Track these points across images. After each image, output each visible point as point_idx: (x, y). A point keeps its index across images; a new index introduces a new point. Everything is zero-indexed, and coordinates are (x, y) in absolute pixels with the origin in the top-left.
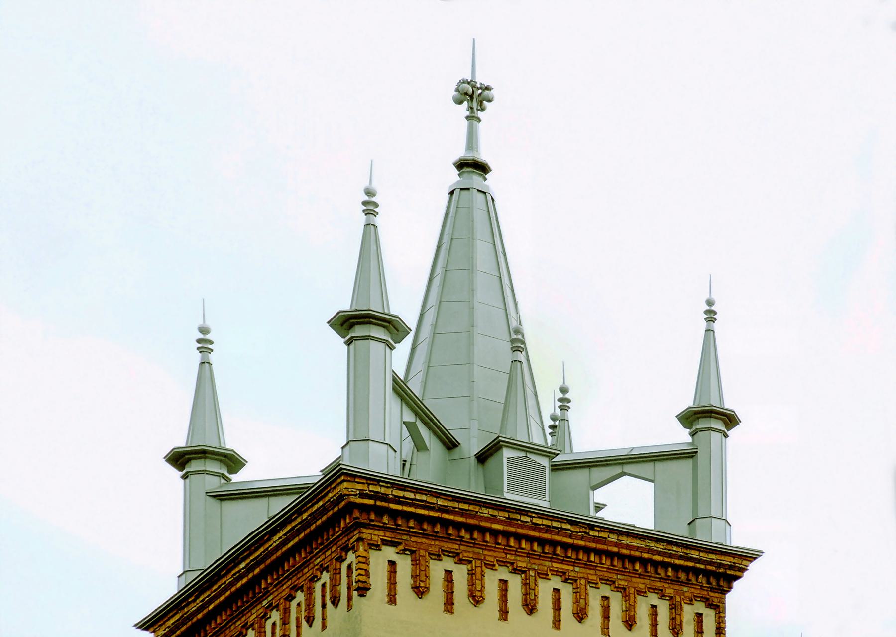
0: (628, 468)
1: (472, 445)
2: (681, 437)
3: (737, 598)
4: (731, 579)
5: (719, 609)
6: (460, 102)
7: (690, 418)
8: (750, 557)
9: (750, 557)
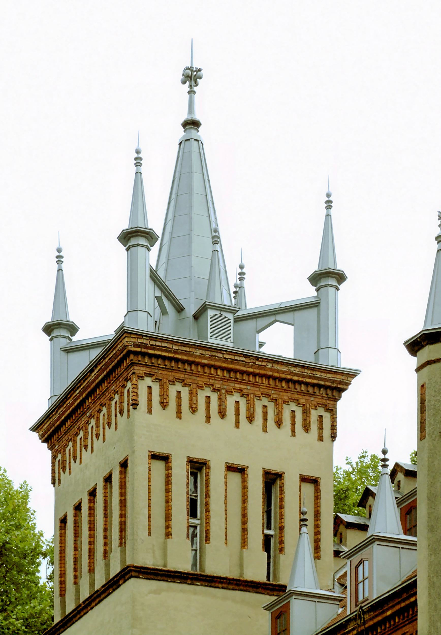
0: (279, 317)
1: (191, 309)
2: (309, 292)
3: (344, 404)
4: (344, 390)
5: (332, 412)
6: (184, 82)
7: (315, 279)
8: (352, 374)
9: (352, 374)
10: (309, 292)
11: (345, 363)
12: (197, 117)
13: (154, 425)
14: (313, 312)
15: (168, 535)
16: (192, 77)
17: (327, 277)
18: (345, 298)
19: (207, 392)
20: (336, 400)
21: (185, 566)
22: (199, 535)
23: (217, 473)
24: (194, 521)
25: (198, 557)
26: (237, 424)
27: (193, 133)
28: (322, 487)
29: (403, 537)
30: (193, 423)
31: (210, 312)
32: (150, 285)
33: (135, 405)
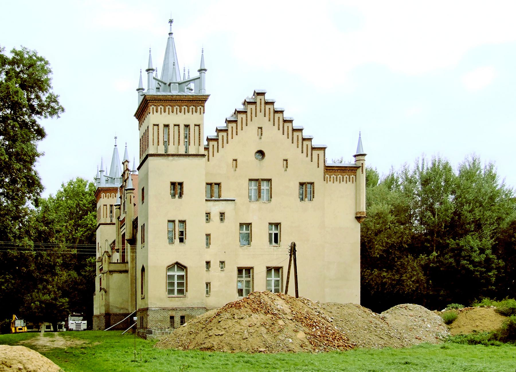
1: (168, 84)
2: (197, 74)
3: (207, 104)
4: (205, 101)
5: (204, 107)
7: (200, 71)
8: (208, 96)
9: (208, 96)
10: (197, 74)
11: (207, 93)
12: (172, 32)
13: (156, 117)
14: (199, 80)
15: (158, 145)
16: (171, 22)
17: (202, 70)
18: (207, 75)
19: (192, 107)
20: (204, 103)
21: (163, 152)
22: (166, 143)
23: (192, 127)
24: (186, 140)
25: (166, 151)
26: (169, 114)
27: (171, 36)
28: (180, 127)
29: (207, 157)
30: (189, 115)
31: (172, 84)
32: (154, 81)
33: (149, 113)
